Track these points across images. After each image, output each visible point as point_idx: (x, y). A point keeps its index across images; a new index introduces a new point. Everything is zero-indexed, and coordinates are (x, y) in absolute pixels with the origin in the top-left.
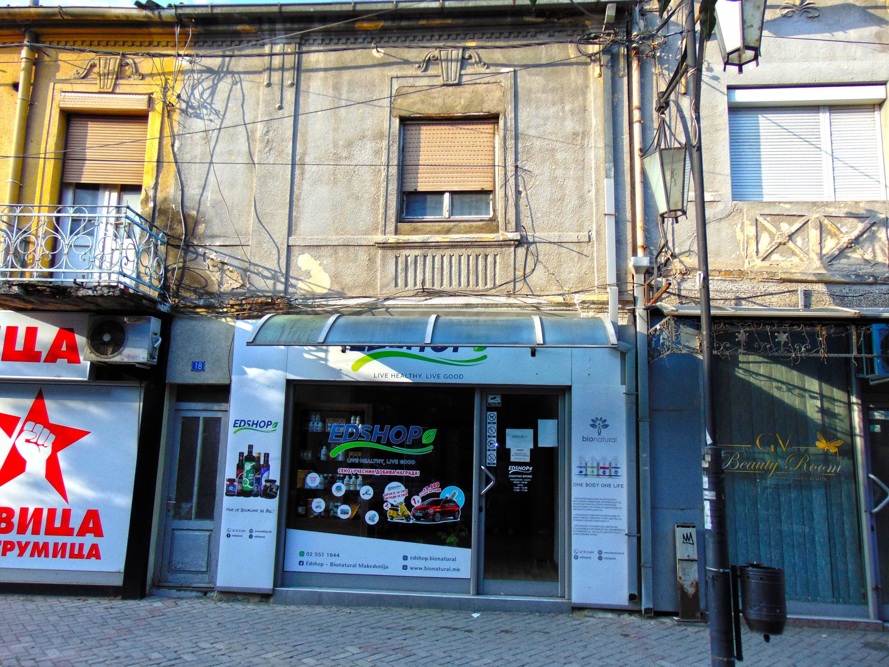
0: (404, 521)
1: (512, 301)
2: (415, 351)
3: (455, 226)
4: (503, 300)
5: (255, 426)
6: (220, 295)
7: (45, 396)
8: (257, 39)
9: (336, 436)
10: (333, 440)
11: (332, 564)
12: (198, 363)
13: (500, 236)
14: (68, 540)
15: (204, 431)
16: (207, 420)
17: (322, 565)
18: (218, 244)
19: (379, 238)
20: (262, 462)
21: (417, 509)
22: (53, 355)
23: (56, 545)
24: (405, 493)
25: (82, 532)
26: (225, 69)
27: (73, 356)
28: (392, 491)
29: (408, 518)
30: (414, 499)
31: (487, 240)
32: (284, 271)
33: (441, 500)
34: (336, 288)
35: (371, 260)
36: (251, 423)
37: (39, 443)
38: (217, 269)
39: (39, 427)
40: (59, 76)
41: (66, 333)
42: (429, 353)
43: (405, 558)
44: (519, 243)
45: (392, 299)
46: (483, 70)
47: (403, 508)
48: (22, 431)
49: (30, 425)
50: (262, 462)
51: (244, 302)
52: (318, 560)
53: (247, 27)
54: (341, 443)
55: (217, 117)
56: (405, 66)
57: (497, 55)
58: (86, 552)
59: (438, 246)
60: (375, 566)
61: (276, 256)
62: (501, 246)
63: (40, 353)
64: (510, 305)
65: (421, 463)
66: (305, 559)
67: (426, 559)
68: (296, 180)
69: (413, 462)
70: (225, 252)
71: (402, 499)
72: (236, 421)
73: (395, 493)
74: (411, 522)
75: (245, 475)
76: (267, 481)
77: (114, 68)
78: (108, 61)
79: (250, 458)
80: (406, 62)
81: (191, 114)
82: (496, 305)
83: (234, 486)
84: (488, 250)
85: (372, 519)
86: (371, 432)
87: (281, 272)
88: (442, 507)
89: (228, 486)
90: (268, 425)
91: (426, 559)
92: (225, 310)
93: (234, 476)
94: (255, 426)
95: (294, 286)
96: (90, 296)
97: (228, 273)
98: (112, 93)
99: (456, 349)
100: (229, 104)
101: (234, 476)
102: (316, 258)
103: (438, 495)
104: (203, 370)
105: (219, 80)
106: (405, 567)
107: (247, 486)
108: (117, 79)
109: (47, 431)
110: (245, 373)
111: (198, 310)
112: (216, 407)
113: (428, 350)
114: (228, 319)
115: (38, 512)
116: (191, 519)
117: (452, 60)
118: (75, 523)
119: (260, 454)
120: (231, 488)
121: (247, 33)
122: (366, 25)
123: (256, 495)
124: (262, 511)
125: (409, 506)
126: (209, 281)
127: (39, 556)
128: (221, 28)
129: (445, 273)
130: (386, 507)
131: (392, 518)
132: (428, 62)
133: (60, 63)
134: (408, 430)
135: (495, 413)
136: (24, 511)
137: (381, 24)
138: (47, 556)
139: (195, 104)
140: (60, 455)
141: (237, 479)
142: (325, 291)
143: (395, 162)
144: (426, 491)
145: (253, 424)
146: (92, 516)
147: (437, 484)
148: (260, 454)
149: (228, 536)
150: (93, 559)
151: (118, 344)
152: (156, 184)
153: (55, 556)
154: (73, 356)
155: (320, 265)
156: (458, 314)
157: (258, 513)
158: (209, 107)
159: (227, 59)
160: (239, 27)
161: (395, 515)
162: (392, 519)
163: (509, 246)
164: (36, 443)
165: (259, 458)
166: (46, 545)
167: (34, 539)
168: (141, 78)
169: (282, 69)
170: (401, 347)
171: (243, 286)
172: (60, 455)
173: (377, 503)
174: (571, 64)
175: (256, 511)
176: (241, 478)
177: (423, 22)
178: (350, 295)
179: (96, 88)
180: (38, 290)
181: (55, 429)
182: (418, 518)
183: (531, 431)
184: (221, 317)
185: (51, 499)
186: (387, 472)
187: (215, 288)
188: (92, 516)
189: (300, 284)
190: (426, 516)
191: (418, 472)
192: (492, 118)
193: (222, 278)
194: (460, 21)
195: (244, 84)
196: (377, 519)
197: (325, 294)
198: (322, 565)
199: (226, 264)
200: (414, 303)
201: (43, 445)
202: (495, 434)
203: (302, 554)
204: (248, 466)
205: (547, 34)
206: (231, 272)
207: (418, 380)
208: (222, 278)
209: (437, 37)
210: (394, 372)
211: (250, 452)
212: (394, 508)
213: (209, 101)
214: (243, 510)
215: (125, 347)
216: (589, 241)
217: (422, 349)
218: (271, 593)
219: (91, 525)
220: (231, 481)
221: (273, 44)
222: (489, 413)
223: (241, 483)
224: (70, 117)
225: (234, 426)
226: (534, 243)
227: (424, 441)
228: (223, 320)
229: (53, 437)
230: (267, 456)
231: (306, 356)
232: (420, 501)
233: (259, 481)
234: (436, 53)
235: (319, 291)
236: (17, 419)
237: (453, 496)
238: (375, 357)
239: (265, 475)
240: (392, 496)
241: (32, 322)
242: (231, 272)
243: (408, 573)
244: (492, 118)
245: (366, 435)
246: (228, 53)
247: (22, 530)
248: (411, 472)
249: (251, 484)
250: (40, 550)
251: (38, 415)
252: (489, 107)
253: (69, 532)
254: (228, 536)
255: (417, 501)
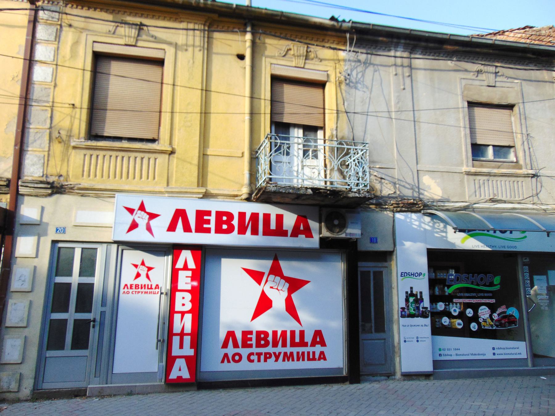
0: (490, 328)
1: (535, 207)
2: (491, 232)
3: (501, 165)
4: (531, 206)
5: (412, 276)
6: (382, 197)
7: (279, 259)
8: (387, 46)
9: (450, 281)
10: (448, 283)
11: (457, 355)
12: (374, 238)
13: (524, 171)
14: (305, 349)
15: (374, 279)
16: (375, 273)
17: (451, 355)
18: (378, 166)
19: (465, 169)
20: (419, 297)
21: (496, 321)
22: (296, 232)
23: (298, 353)
24: (489, 312)
25: (313, 344)
26: (369, 62)
27: (308, 233)
28: (483, 311)
29: (492, 326)
30: (494, 315)
31: (519, 173)
32: (417, 185)
33: (507, 315)
34: (446, 196)
35: (462, 181)
36: (410, 274)
37: (278, 289)
38: (377, 182)
39: (278, 278)
40: (267, 53)
41: (302, 219)
42: (498, 234)
43: (494, 349)
44: (534, 176)
45: (477, 203)
46: (505, 80)
47: (489, 320)
48: (267, 281)
49: (272, 277)
50: (419, 297)
51: (400, 202)
52: (449, 353)
53: (385, 39)
54: (453, 285)
55: (367, 90)
56: (466, 73)
57: (510, 72)
58: (317, 356)
59: (495, 175)
60: (479, 354)
61: (412, 176)
62: (525, 177)
63: (287, 231)
64: (534, 209)
65: (494, 295)
66: (442, 352)
67: (504, 349)
68: (417, 132)
69: (490, 295)
70: (382, 172)
71: (487, 316)
72: (402, 273)
73: (484, 312)
74: (494, 328)
75: (410, 305)
76: (423, 308)
77: (303, 53)
78: (299, 48)
79: (412, 295)
80: (466, 71)
81: (352, 86)
82: (527, 209)
83: (405, 312)
84: (519, 179)
85: (474, 328)
86: (468, 278)
87: (415, 186)
88: (508, 319)
89: (401, 312)
90: (420, 275)
91: (504, 349)
92: (387, 207)
93: (404, 306)
94: (412, 276)
95: (423, 194)
96: (357, 197)
97: (384, 184)
98: (303, 68)
99: (511, 232)
100: (374, 83)
101: (404, 306)
102: (433, 178)
103: (505, 312)
104: (377, 242)
105: (366, 68)
106: (440, 355)
107: (412, 311)
108: (306, 59)
109: (283, 281)
110: (404, 245)
111: (371, 206)
112: (380, 264)
113: (498, 232)
114: (388, 212)
115: (284, 333)
116: (372, 333)
117: (131, 37)
118: (308, 338)
119: (417, 292)
120: (403, 313)
121: (382, 42)
122: (449, 47)
123: (417, 317)
124: (422, 326)
125: (492, 319)
126: (374, 189)
127: (288, 360)
128: (370, 37)
129: (98, 167)
130: (481, 320)
131: (484, 326)
132: (479, 72)
133: (267, 45)
134: (486, 276)
135: (527, 267)
136: (275, 333)
137: (457, 48)
138: (293, 360)
139: (354, 81)
140: (293, 296)
141: (406, 308)
142: (439, 198)
143: (468, 126)
144: (499, 311)
145: (411, 274)
146: (318, 333)
147: (504, 306)
148: (417, 292)
149: (405, 341)
150: (322, 360)
151: (343, 226)
152: (337, 127)
153: (298, 359)
154: (308, 233)
155: (435, 182)
156: (508, 212)
157: (420, 327)
158: (362, 83)
159: (369, 56)
160: (381, 39)
161: (485, 325)
162: (484, 327)
163: (529, 177)
164: (277, 289)
165: (417, 294)
166: (292, 354)
167: (283, 350)
168: (320, 60)
169: (402, 66)
170: (484, 230)
171: (395, 192)
172: (293, 296)
173: (475, 318)
174: (546, 82)
175: (419, 326)
176: (408, 307)
177: (478, 50)
178: (452, 200)
179: (294, 64)
180: (320, 192)
181: (288, 279)
182: (497, 326)
183: (545, 277)
184: (384, 211)
185: (290, 325)
186: (479, 301)
187: (378, 194)
188: (318, 333)
189: (426, 193)
190: (501, 325)
191: (494, 300)
192: (510, 107)
193: (381, 187)
194: (497, 52)
195: (381, 72)
196: (477, 327)
197: (440, 199)
198: (451, 355)
199: (384, 179)
200: (488, 206)
201: (282, 290)
202: (529, 279)
203: (440, 350)
204: (411, 299)
205: (534, 64)
206: (386, 184)
207: (495, 249)
208: (381, 187)
209: (336, 42)
210: (482, 245)
211: (412, 291)
212: (485, 321)
213: (362, 79)
214: (411, 326)
215: (347, 228)
216: (242, 156)
217: (495, 232)
218: (432, 373)
219: (318, 340)
220: (403, 309)
221: (396, 51)
222: (524, 267)
223: (408, 309)
224: (276, 80)
225: (401, 276)
226: (539, 176)
227: (495, 283)
228: (385, 212)
229: (287, 285)
230: (421, 293)
231: (436, 235)
232: (497, 316)
233: (418, 308)
234: (482, 67)
235: (436, 197)
236: (262, 274)
237: (513, 313)
238: (472, 236)
239: (422, 304)
240: (483, 314)
241: (280, 211)
242: (386, 184)
243: (496, 357)
244: (510, 107)
245: (465, 280)
246: (369, 52)
247: (275, 345)
248: (491, 300)
249: (414, 310)
250: (288, 357)
251: (276, 271)
252: (510, 101)
253: (305, 345)
254: (405, 341)
255: (495, 316)
